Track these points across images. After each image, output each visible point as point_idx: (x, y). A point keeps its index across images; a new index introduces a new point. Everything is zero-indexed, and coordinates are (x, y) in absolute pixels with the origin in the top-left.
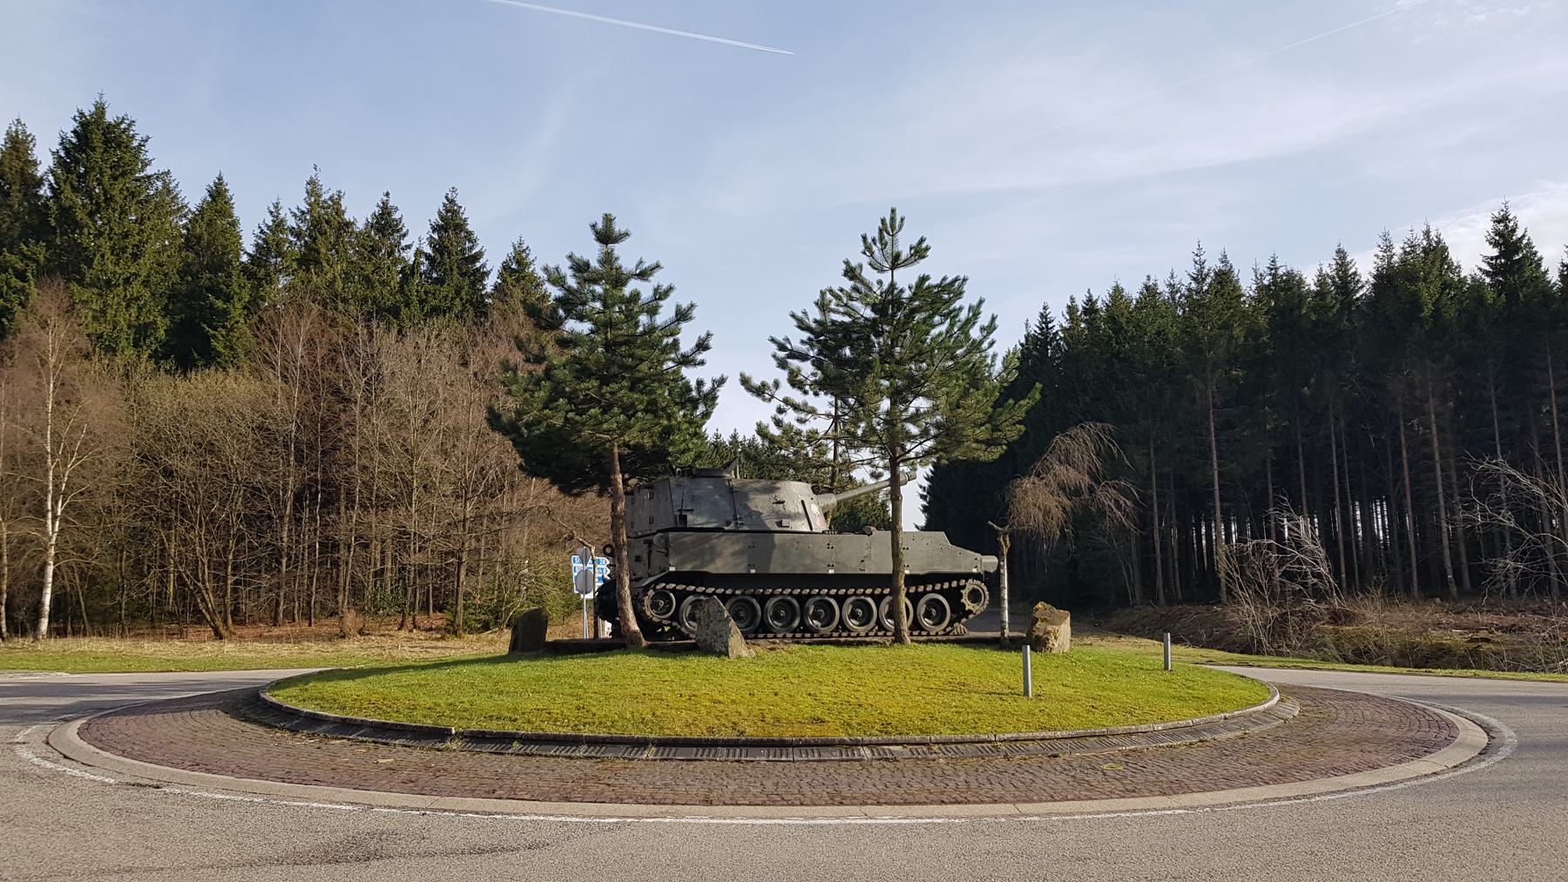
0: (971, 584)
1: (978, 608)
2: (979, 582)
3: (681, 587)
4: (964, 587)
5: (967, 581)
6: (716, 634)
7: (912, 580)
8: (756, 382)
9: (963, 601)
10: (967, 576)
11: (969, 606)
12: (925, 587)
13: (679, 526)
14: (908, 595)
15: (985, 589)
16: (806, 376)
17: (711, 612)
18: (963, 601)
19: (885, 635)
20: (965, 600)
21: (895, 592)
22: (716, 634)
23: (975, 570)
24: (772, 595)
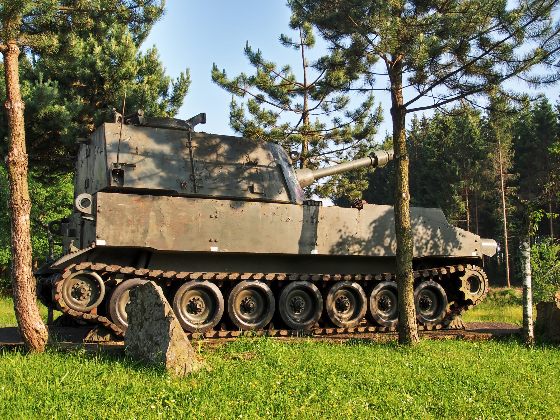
0: (471, 271)
1: (477, 297)
2: (478, 268)
3: (112, 268)
4: (463, 273)
5: (465, 266)
6: (151, 339)
7: (418, 263)
8: (231, 78)
9: (461, 289)
10: (465, 261)
11: (468, 295)
12: (332, 276)
13: (114, 184)
14: (89, 269)
15: (485, 275)
16: (278, 73)
17: (146, 303)
18: (461, 289)
19: (377, 331)
20: (465, 288)
21: (401, 279)
22: (151, 339)
23: (474, 254)
24: (239, 280)
